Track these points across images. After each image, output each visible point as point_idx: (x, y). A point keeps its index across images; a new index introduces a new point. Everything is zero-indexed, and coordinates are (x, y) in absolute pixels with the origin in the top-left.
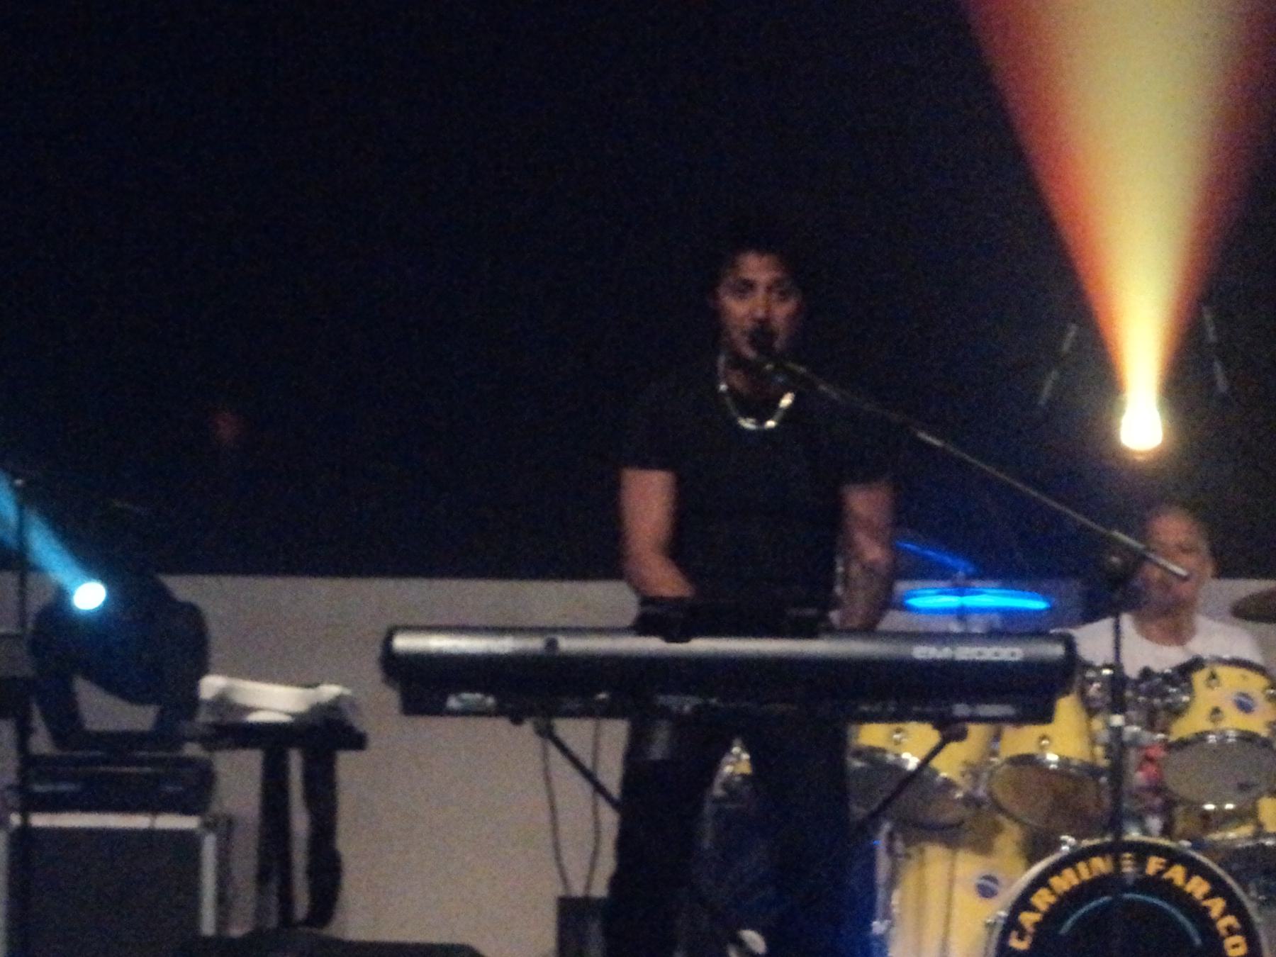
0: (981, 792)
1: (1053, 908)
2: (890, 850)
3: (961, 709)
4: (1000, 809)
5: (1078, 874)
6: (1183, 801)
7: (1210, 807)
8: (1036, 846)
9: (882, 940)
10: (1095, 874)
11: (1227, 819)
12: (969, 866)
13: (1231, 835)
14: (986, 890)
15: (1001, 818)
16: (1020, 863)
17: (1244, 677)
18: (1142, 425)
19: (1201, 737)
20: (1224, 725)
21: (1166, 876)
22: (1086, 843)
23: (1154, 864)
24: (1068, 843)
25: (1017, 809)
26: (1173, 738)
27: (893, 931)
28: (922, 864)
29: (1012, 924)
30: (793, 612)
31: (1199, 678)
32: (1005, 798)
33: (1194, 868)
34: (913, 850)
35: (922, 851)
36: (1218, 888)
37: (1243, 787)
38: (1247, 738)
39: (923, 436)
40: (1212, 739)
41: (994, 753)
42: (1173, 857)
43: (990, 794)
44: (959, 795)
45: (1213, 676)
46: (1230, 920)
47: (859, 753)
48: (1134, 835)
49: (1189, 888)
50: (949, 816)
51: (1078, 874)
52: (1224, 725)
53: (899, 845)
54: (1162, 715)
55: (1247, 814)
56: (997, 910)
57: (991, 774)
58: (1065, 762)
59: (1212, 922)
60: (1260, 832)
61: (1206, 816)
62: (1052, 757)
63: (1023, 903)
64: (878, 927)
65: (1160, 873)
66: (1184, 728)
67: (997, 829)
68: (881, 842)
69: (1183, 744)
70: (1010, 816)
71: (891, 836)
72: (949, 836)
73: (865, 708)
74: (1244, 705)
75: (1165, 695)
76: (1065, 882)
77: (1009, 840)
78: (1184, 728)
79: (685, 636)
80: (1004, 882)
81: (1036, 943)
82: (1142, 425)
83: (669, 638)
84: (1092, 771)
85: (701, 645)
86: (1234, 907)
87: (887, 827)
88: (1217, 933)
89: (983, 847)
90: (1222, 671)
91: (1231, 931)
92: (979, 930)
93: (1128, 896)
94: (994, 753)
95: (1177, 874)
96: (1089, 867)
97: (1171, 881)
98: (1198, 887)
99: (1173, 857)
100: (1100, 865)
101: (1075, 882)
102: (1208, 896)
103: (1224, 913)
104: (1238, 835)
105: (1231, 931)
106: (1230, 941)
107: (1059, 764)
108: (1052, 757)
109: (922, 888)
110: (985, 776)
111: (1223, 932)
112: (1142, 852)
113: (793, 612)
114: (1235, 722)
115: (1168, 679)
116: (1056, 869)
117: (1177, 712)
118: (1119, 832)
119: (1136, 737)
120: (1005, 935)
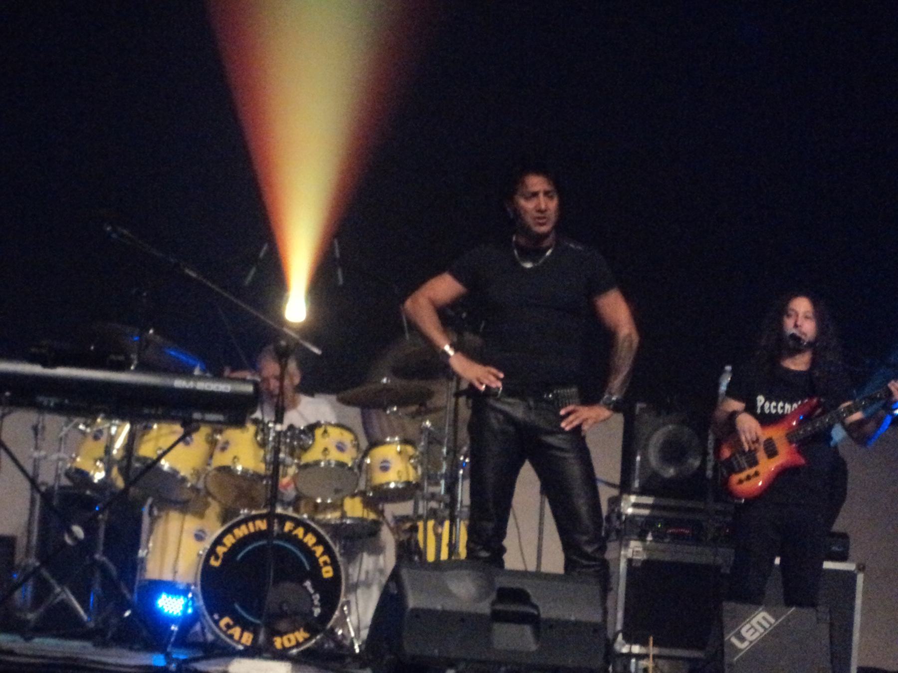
0: (200, 485)
1: (234, 545)
2: (150, 513)
3: (197, 416)
4: (208, 494)
5: (248, 528)
6: (305, 497)
7: (319, 501)
8: (226, 515)
9: (143, 560)
10: (257, 529)
11: (326, 507)
12: (191, 524)
13: (329, 516)
14: (199, 537)
15: (210, 499)
16: (219, 524)
17: (342, 434)
18: (296, 309)
19: (317, 463)
20: (328, 458)
21: (295, 532)
22: (254, 512)
23: (288, 526)
24: (244, 512)
25: (219, 497)
26: (302, 463)
27: (150, 556)
28: (167, 521)
29: (212, 552)
30: (113, 357)
31: (319, 432)
32: (212, 489)
33: (308, 529)
34: (163, 514)
35: (167, 514)
36: (320, 541)
37: (337, 491)
38: (341, 465)
39: (187, 271)
40: (322, 464)
41: (209, 464)
42: (298, 523)
43: (205, 487)
44: (189, 485)
45: (325, 432)
46: (326, 558)
47: (139, 459)
48: (279, 510)
49: (306, 540)
50: (185, 497)
51: (248, 528)
52: (328, 458)
53: (156, 512)
54: (297, 451)
55: (338, 506)
56: (207, 544)
57: (207, 475)
58: (245, 472)
59: (316, 560)
60: (344, 516)
61: (316, 506)
62: (239, 468)
63: (218, 541)
64: (141, 553)
65: (290, 531)
66: (309, 457)
67: (207, 505)
68: (146, 510)
69: (307, 466)
70: (214, 498)
71: (151, 507)
72: (184, 507)
73: (146, 411)
74: (341, 448)
75: (300, 439)
76: (241, 532)
77: (214, 510)
78: (309, 457)
79: (54, 364)
80: (209, 534)
81: (222, 565)
82: (296, 309)
83: (45, 365)
84: (257, 477)
85: (62, 371)
86: (328, 551)
87: (150, 501)
88: (318, 564)
89: (201, 515)
90: (331, 430)
91: (325, 563)
92: (194, 557)
93: (276, 542)
94: (209, 464)
95: (300, 532)
96: (254, 526)
97: (296, 536)
98: (310, 540)
99: (298, 523)
100: (262, 525)
101: (246, 532)
102: (315, 545)
103: (323, 554)
104: (332, 516)
105: (325, 563)
106: (324, 570)
107: (242, 472)
108: (239, 468)
109: (165, 533)
110: (203, 476)
111: (322, 564)
112: (283, 519)
113: (113, 357)
114: (335, 456)
115: (303, 432)
116: (238, 525)
117: (305, 449)
118: (273, 507)
119: (284, 459)
120: (207, 560)
